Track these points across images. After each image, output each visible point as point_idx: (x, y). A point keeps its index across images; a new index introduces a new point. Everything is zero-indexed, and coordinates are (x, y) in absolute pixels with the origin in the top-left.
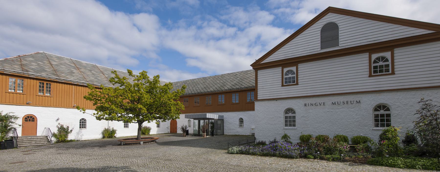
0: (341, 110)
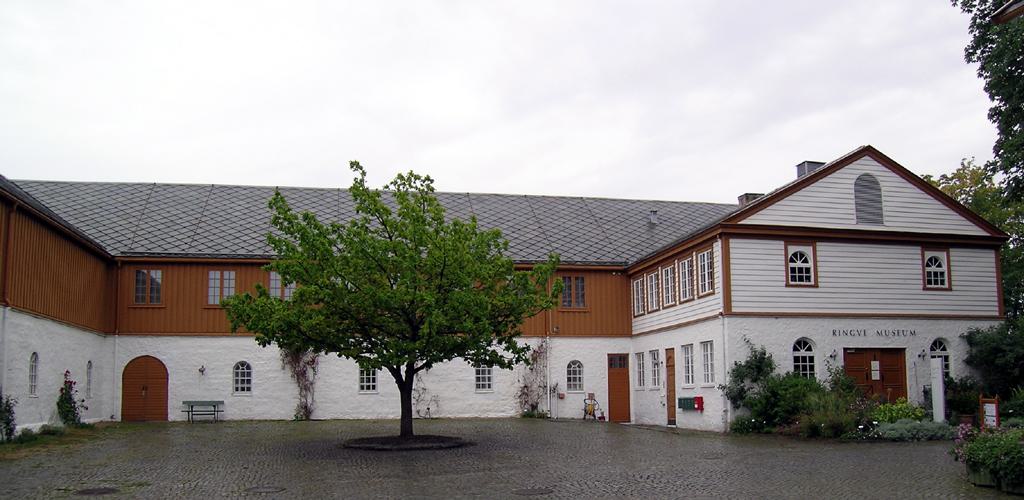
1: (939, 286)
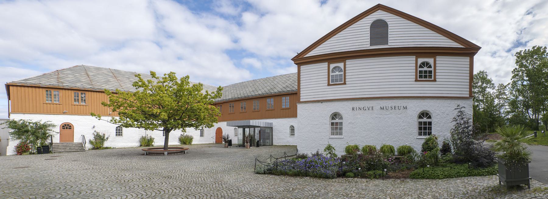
0: (389, 116)
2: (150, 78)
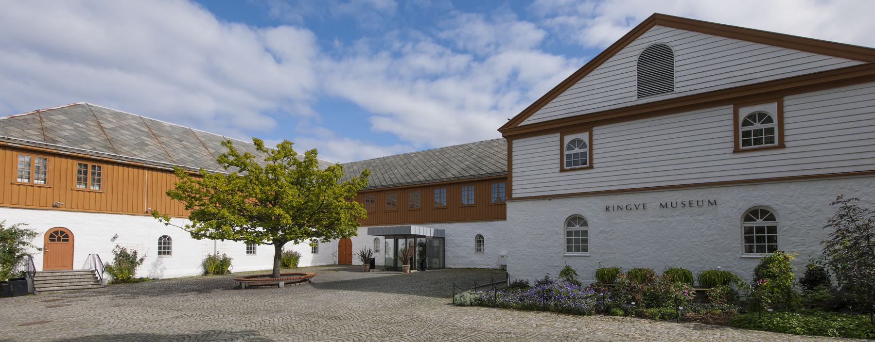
0: (678, 218)
1: (741, 139)
2: (253, 150)
